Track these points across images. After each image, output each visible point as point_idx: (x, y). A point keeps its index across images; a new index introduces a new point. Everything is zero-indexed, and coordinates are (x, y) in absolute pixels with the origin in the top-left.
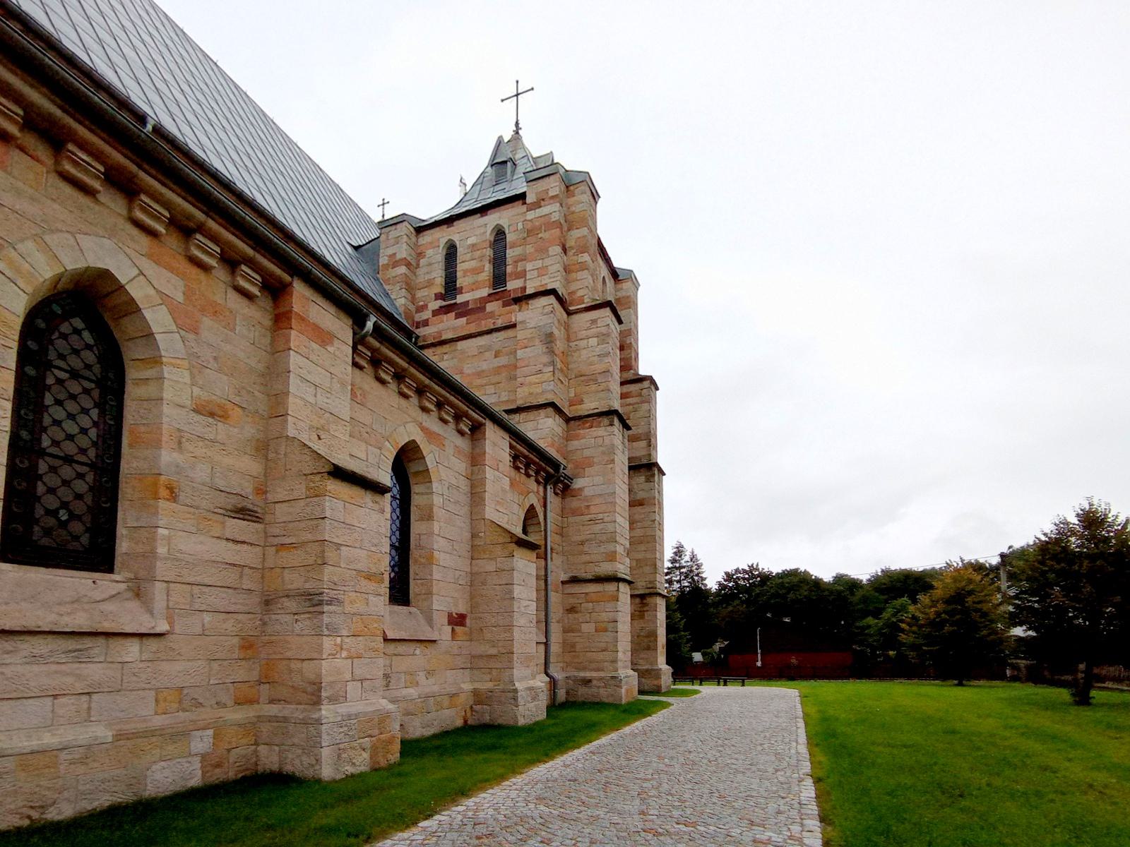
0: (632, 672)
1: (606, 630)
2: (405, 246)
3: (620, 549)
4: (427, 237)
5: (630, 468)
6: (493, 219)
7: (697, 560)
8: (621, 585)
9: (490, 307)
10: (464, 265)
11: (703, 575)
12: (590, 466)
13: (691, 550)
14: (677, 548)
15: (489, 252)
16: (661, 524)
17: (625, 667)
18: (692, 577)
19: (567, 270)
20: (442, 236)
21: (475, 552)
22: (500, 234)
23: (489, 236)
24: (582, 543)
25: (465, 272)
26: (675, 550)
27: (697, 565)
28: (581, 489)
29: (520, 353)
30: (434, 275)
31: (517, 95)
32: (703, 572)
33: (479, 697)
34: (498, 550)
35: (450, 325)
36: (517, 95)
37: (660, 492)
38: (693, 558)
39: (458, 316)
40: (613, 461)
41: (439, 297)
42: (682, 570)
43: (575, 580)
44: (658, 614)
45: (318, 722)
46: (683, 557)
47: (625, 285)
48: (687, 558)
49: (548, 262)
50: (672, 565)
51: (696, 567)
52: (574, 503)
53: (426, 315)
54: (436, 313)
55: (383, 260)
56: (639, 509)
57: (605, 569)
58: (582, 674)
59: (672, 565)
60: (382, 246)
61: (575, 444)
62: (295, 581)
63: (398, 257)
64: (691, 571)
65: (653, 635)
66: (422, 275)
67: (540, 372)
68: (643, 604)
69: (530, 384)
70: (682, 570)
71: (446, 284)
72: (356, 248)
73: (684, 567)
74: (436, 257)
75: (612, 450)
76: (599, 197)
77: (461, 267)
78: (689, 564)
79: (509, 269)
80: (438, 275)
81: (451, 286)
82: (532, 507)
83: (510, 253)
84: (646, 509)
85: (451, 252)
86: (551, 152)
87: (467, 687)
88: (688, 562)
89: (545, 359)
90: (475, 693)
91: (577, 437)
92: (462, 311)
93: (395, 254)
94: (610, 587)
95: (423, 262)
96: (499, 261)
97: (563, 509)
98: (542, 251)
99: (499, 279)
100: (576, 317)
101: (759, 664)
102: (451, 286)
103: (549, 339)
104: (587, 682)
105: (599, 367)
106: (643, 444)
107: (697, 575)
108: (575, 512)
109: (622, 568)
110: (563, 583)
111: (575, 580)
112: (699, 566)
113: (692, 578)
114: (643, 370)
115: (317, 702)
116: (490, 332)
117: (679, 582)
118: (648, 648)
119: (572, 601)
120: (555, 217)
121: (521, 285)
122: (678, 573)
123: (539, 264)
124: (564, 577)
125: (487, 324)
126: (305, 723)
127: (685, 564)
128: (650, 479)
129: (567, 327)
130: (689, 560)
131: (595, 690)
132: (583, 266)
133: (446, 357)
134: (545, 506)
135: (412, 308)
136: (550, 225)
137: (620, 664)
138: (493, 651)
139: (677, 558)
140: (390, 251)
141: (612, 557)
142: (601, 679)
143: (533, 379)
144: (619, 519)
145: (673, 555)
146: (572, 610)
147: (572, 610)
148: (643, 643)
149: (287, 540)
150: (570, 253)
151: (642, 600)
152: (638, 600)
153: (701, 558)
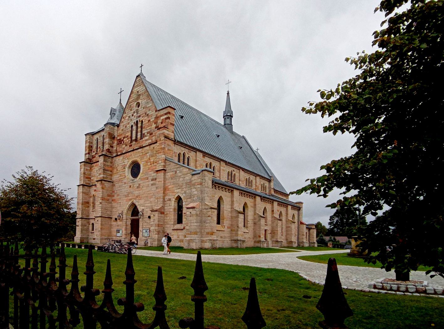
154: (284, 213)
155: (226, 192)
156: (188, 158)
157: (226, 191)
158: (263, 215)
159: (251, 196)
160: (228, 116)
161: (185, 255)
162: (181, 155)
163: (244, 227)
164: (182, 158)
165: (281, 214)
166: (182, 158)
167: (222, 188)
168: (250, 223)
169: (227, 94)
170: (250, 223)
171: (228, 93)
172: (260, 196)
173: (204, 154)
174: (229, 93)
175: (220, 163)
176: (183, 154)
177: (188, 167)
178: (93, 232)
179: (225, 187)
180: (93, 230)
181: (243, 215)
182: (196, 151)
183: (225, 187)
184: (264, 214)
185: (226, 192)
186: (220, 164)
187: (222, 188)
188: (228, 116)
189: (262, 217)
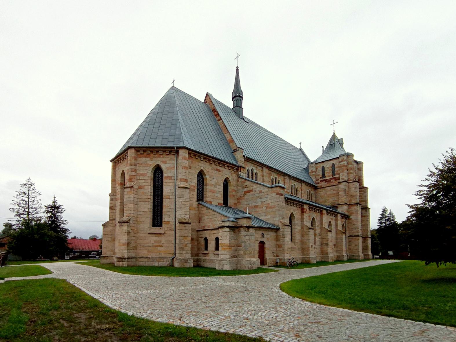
0: (362, 254)
1: (357, 246)
2: (314, 168)
3: (359, 230)
4: (318, 165)
5: (361, 209)
6: (332, 162)
7: (392, 214)
8: (360, 237)
9: (332, 180)
10: (326, 171)
11: (395, 220)
12: (353, 214)
13: (389, 210)
14: (384, 209)
15: (331, 169)
16: (369, 221)
17: (361, 253)
18: (391, 221)
19: (348, 174)
20: (322, 165)
21: (337, 234)
22: (333, 165)
23: (331, 165)
24: (352, 229)
25: (327, 173)
26: (383, 210)
27: (392, 216)
28: (351, 218)
29: (339, 193)
30: (320, 173)
31: (334, 124)
32: (395, 219)
33: (338, 256)
34: (340, 234)
35: (324, 184)
36: (334, 124)
37: (369, 214)
38: (391, 213)
39: (325, 182)
40: (358, 213)
41: (321, 178)
42: (386, 218)
43: (351, 236)
44: (369, 242)
45: (329, 256)
46: (386, 213)
47: (360, 165)
48: (388, 213)
49: (344, 173)
50: (382, 216)
51: (392, 217)
52: (350, 221)
53: (319, 181)
54: (321, 181)
55: (310, 171)
56: (363, 218)
57: (356, 234)
58: (352, 254)
59: (382, 216)
60: (309, 167)
61: (350, 209)
62: (325, 242)
63: (313, 170)
64: (390, 219)
65: (367, 247)
66: (318, 173)
67: (344, 197)
68: (365, 239)
69: (342, 199)
70: (386, 218)
71: (322, 175)
72: (304, 169)
73: (387, 217)
74: (320, 169)
75: (358, 210)
76: (354, 155)
77: (326, 172)
78: (389, 216)
79: (336, 173)
80: (321, 173)
81: (323, 176)
82: (343, 224)
83: (336, 169)
84: (366, 218)
85: (323, 167)
86: (342, 138)
87: (336, 255)
88: (388, 215)
89: (344, 195)
90: (337, 256)
91: (351, 208)
92: (326, 181)
93: (312, 170)
94: (357, 238)
95: (317, 170)
96: (333, 171)
97: (348, 222)
98: (343, 171)
99: (334, 174)
100: (350, 184)
101: (409, 255)
102: (323, 176)
103: (345, 190)
104: (353, 256)
105: (355, 194)
106: (365, 202)
107: (393, 220)
108: (350, 223)
109: (360, 233)
110: (348, 236)
111: (351, 236)
112: (393, 217)
113: (390, 221)
114: (365, 185)
115: (328, 255)
116: (332, 186)
117: (384, 223)
118: (366, 249)
119: (350, 240)
120: (345, 164)
121: (338, 176)
122: (385, 219)
123: (342, 174)
124: (349, 235)
125: (332, 184)
126: (327, 256)
127: (387, 216)
128: (366, 211)
129: (348, 186)
130: (389, 214)
131: (355, 257)
132: (351, 173)
133: (323, 191)
134: (345, 223)
135: (316, 180)
136: (344, 166)
137: (360, 252)
138: (340, 249)
139: (384, 213)
140: (311, 169)
141: (358, 232)
142: (356, 255)
143: (342, 198)
144: (359, 224)
145: (382, 212)
146: (350, 242)
147: (350, 242)
148: (365, 248)
149: (324, 238)
150: (348, 170)
151: (365, 238)
152: (364, 239)
153: (394, 213)
154: (317, 220)
155: (288, 205)
156: (256, 174)
157: (288, 204)
158: (310, 227)
159: (316, 210)
160: (237, 96)
161: (240, 277)
162: (249, 170)
163: (291, 241)
164: (250, 174)
165: (313, 221)
166: (250, 174)
167: (331, 213)
168: (298, 237)
169: (236, 71)
170: (298, 237)
171: (237, 70)
172: (327, 210)
173: (270, 169)
174: (239, 69)
175: (301, 184)
176: (252, 170)
177: (296, 196)
178: (206, 252)
179: (299, 203)
180: (217, 248)
181: (290, 228)
182: (263, 166)
183: (299, 203)
184: (312, 226)
185: (288, 205)
186: (301, 185)
187: (331, 213)
188: (237, 96)
189: (310, 228)
